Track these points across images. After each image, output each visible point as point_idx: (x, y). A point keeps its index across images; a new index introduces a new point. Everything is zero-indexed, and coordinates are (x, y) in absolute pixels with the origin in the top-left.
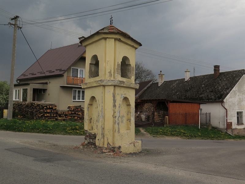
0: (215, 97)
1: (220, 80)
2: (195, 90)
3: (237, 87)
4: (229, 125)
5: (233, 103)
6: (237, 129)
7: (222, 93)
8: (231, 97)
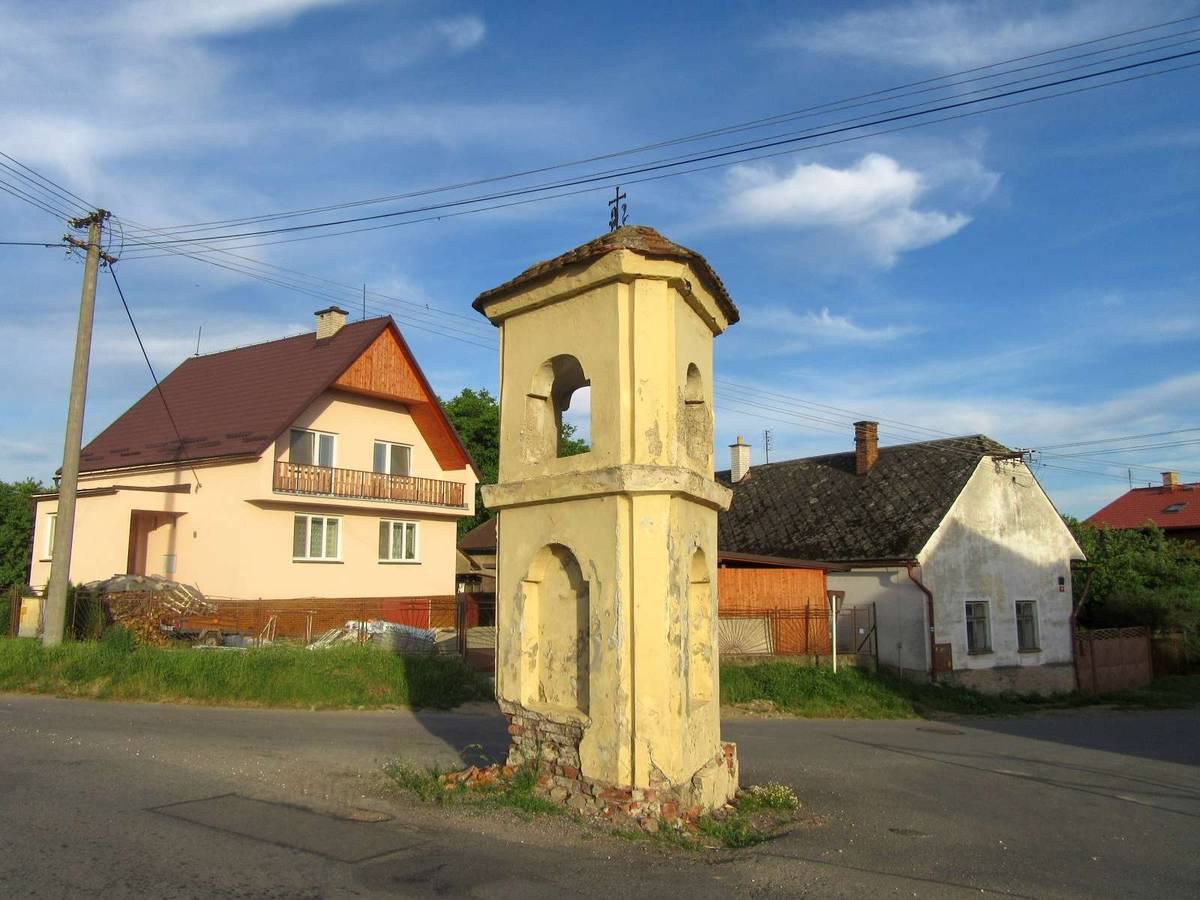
0: (876, 544)
1: (885, 478)
2: (783, 517)
3: (962, 506)
4: (941, 656)
6: (971, 670)
7: (903, 526)
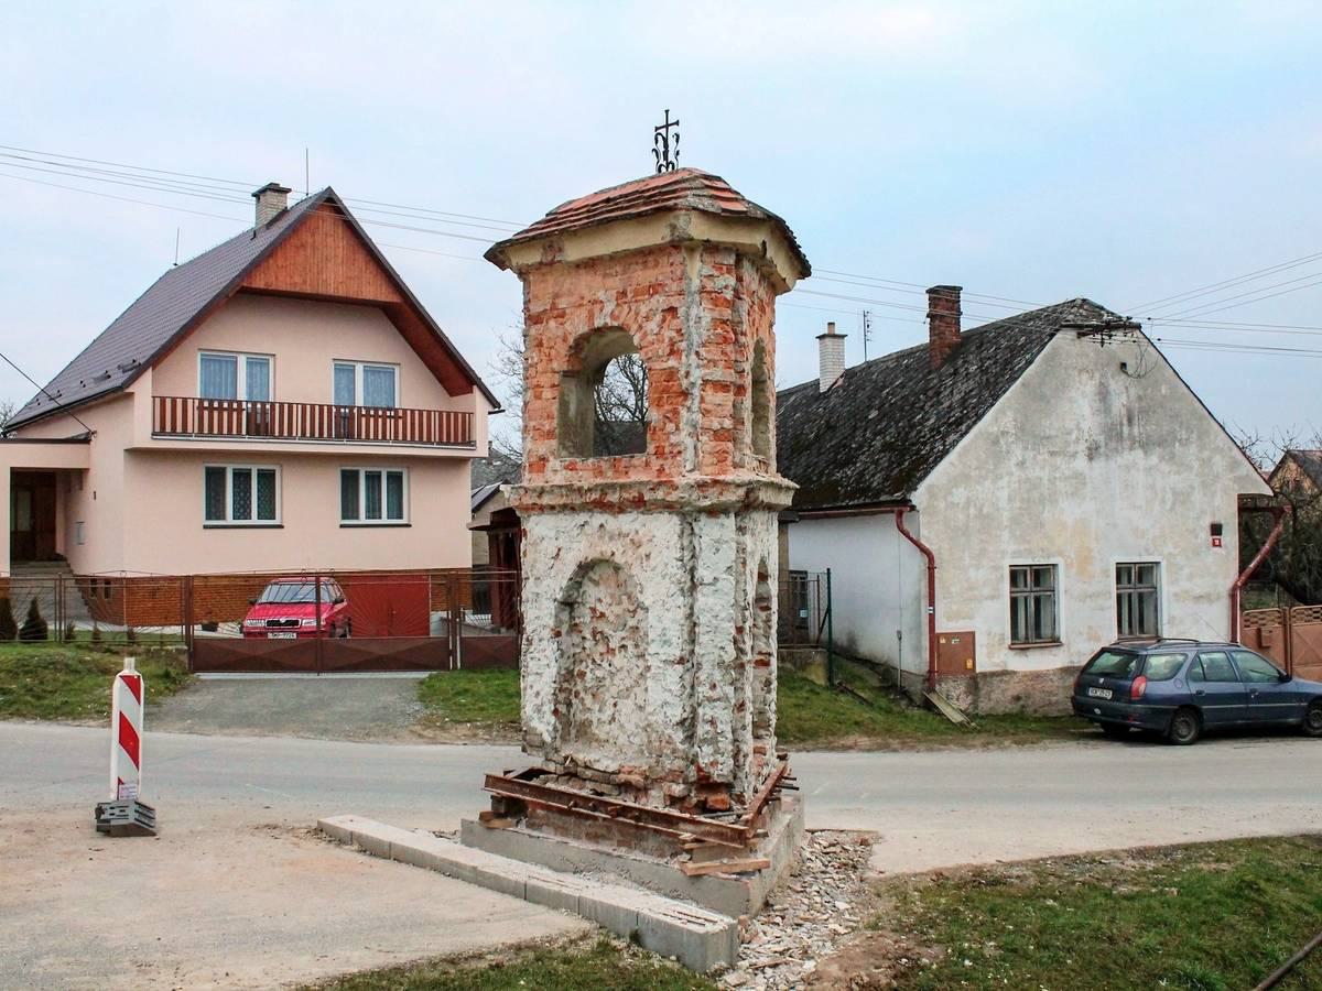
5: (980, 515)
6: (1014, 673)
8: (965, 478)
